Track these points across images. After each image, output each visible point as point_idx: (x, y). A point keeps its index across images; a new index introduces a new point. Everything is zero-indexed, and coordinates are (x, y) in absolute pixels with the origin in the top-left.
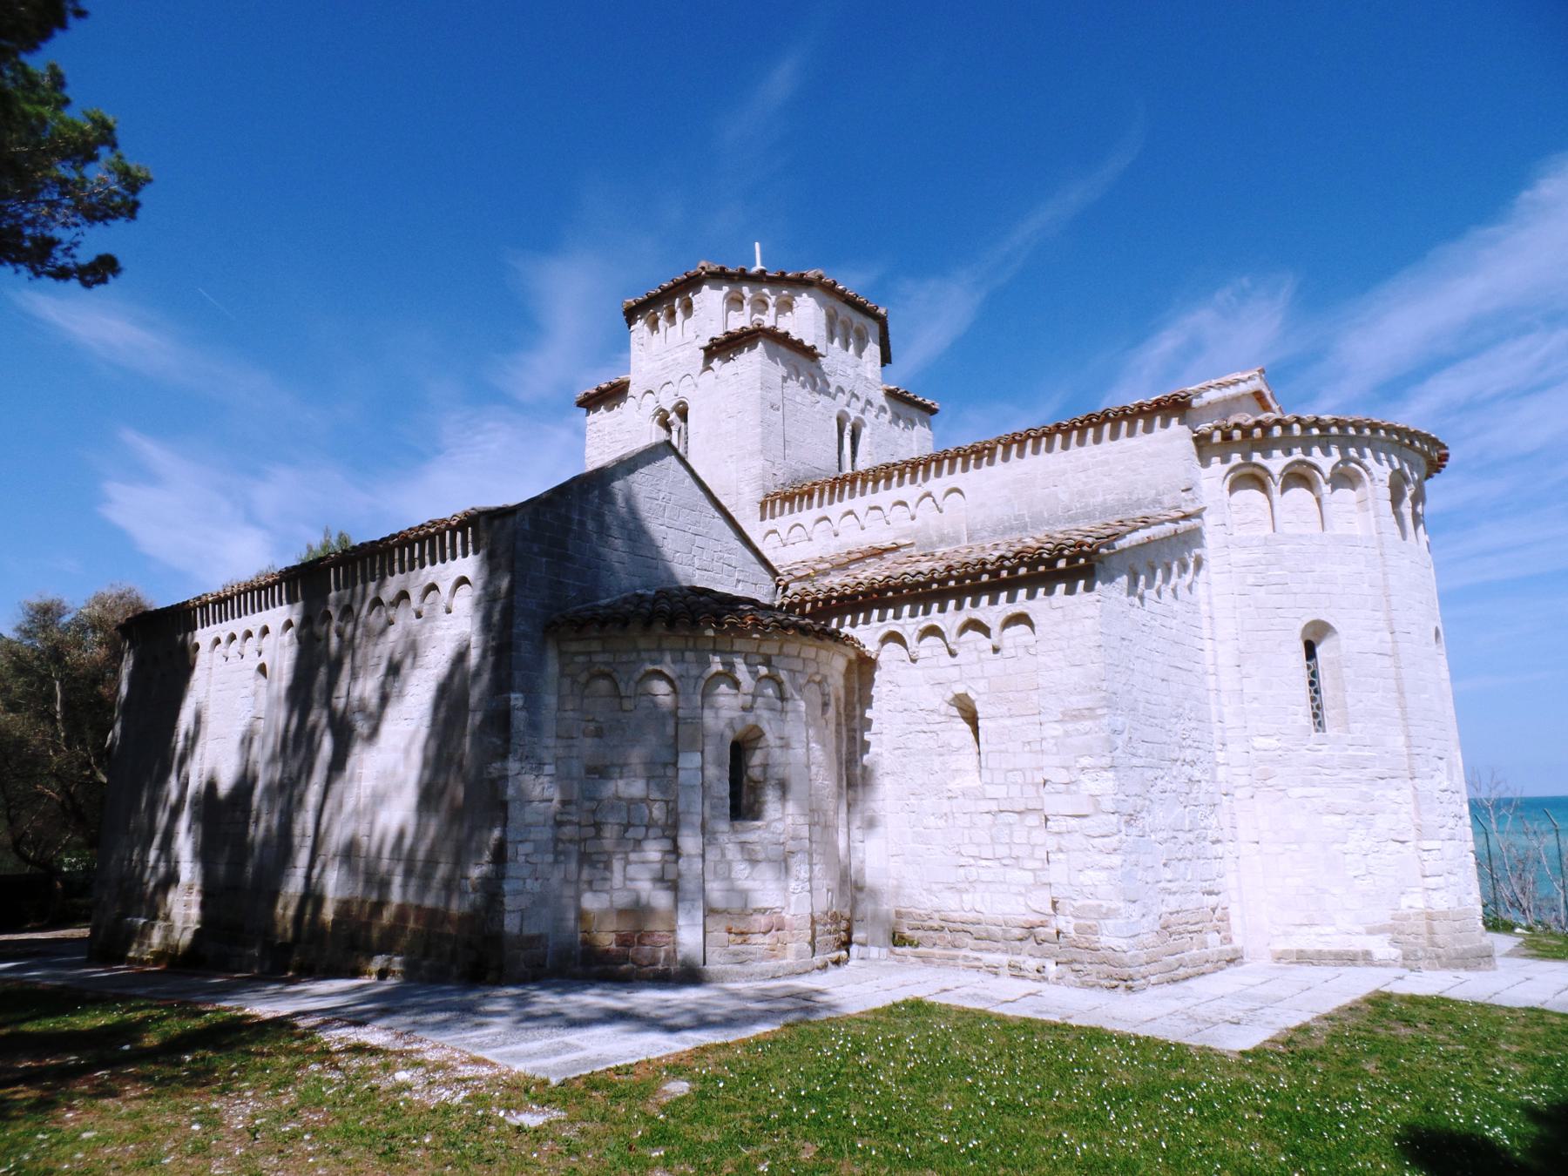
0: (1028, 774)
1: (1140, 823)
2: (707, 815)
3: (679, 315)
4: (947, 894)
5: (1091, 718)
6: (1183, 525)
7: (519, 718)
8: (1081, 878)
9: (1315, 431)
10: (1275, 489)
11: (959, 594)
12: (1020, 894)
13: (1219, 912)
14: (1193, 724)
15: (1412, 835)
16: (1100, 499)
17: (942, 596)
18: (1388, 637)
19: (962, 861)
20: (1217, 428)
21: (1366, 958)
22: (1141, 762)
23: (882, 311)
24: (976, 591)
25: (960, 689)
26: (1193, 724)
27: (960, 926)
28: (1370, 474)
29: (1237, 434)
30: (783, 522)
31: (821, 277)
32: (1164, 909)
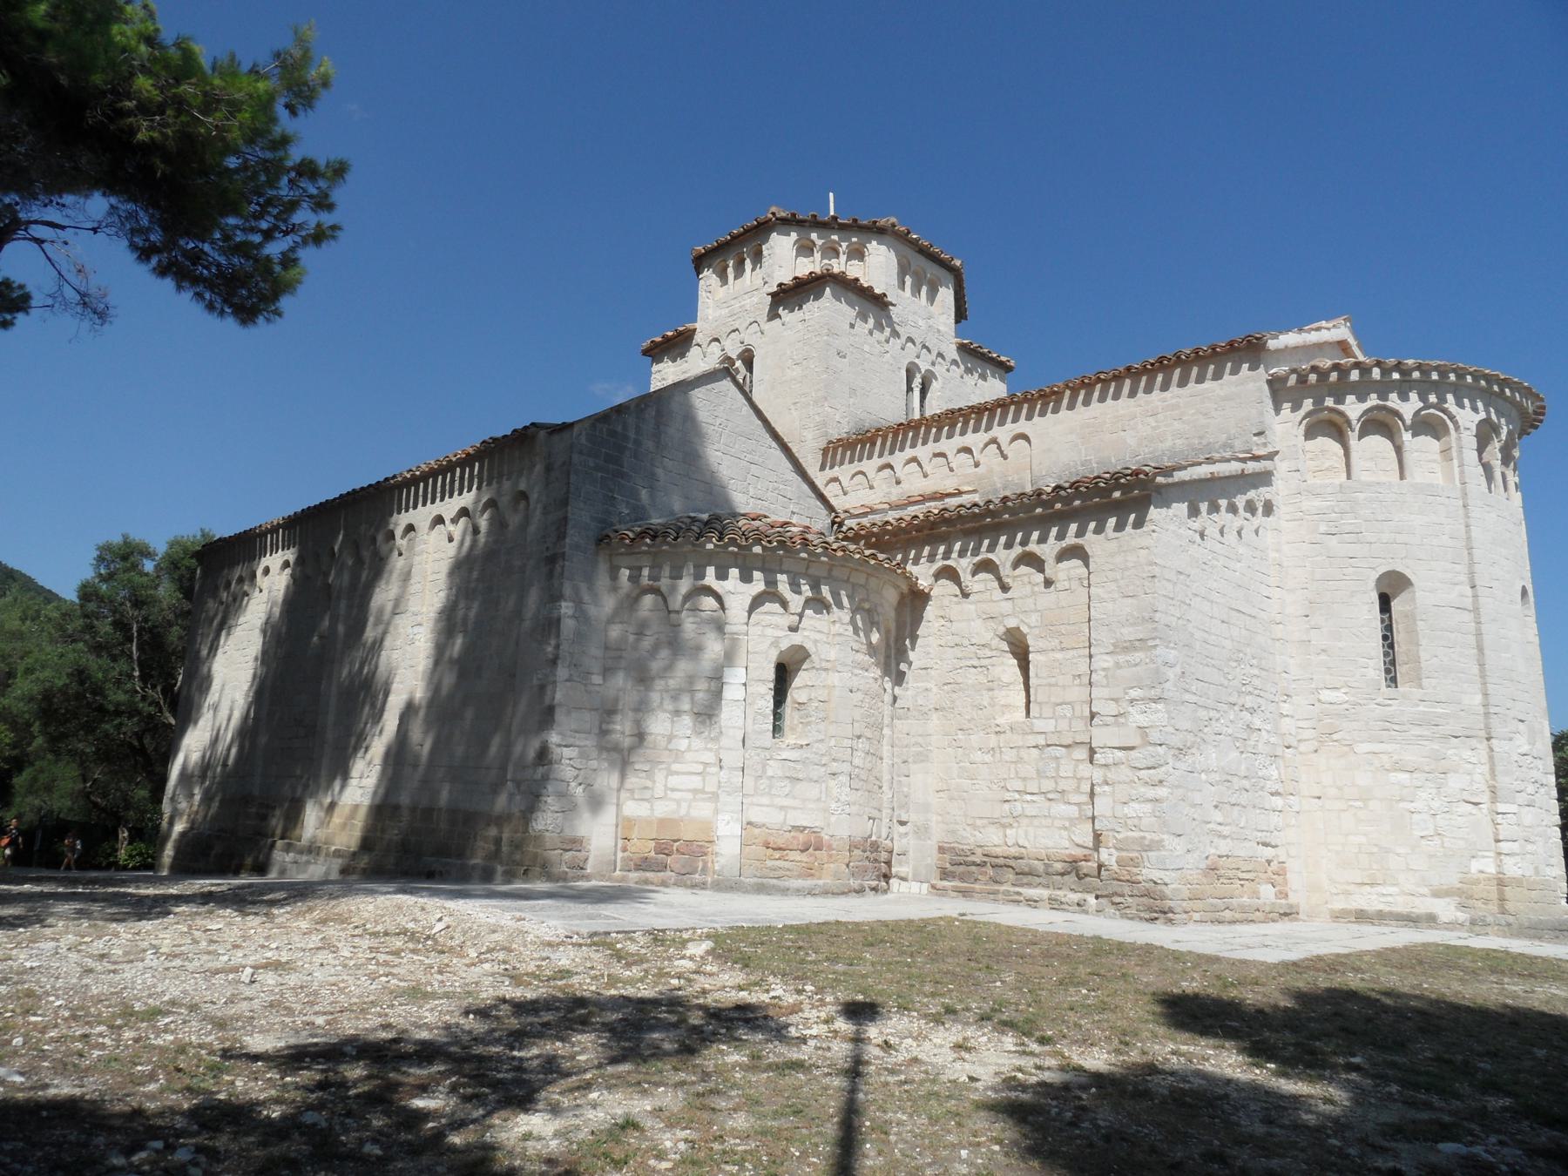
0: (1078, 708)
1: (1189, 759)
2: (749, 729)
3: (748, 264)
4: (992, 829)
5: (1141, 649)
6: (1251, 467)
8: (1126, 810)
9: (1396, 376)
10: (1353, 437)
11: (1009, 528)
12: (1065, 828)
13: (1274, 865)
14: (1256, 672)
15: (1485, 798)
16: (1169, 444)
17: (995, 530)
18: (1469, 592)
19: (1007, 796)
20: (1293, 371)
21: (1431, 920)
22: (1194, 699)
23: (958, 263)
24: (1028, 524)
25: (1012, 623)
26: (1256, 672)
27: (1001, 861)
28: (1456, 423)
29: (1313, 378)
30: (844, 472)
31: (893, 225)
32: (1213, 851)
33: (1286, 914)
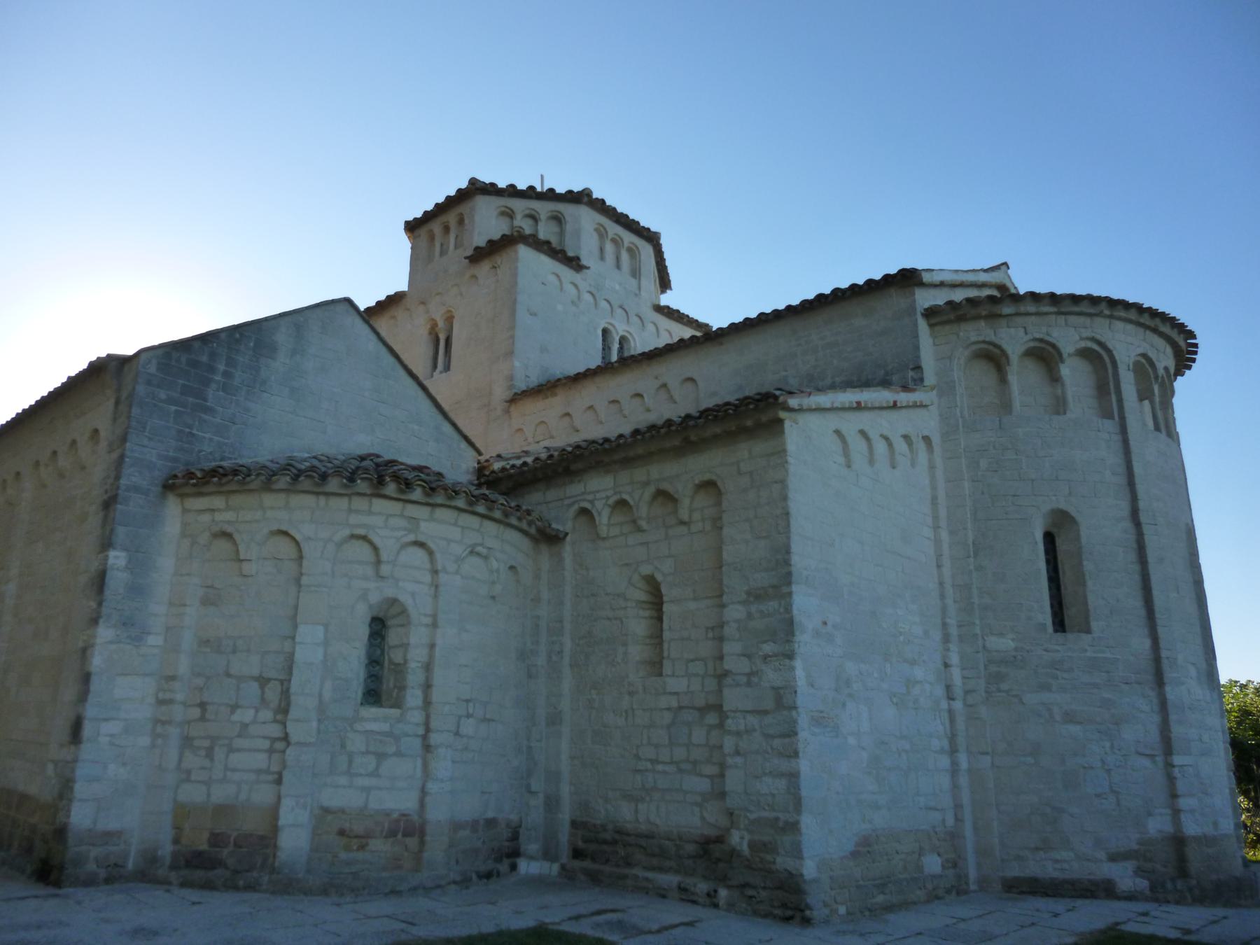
7: (118, 579)
25: (646, 570)
33: (920, 934)
